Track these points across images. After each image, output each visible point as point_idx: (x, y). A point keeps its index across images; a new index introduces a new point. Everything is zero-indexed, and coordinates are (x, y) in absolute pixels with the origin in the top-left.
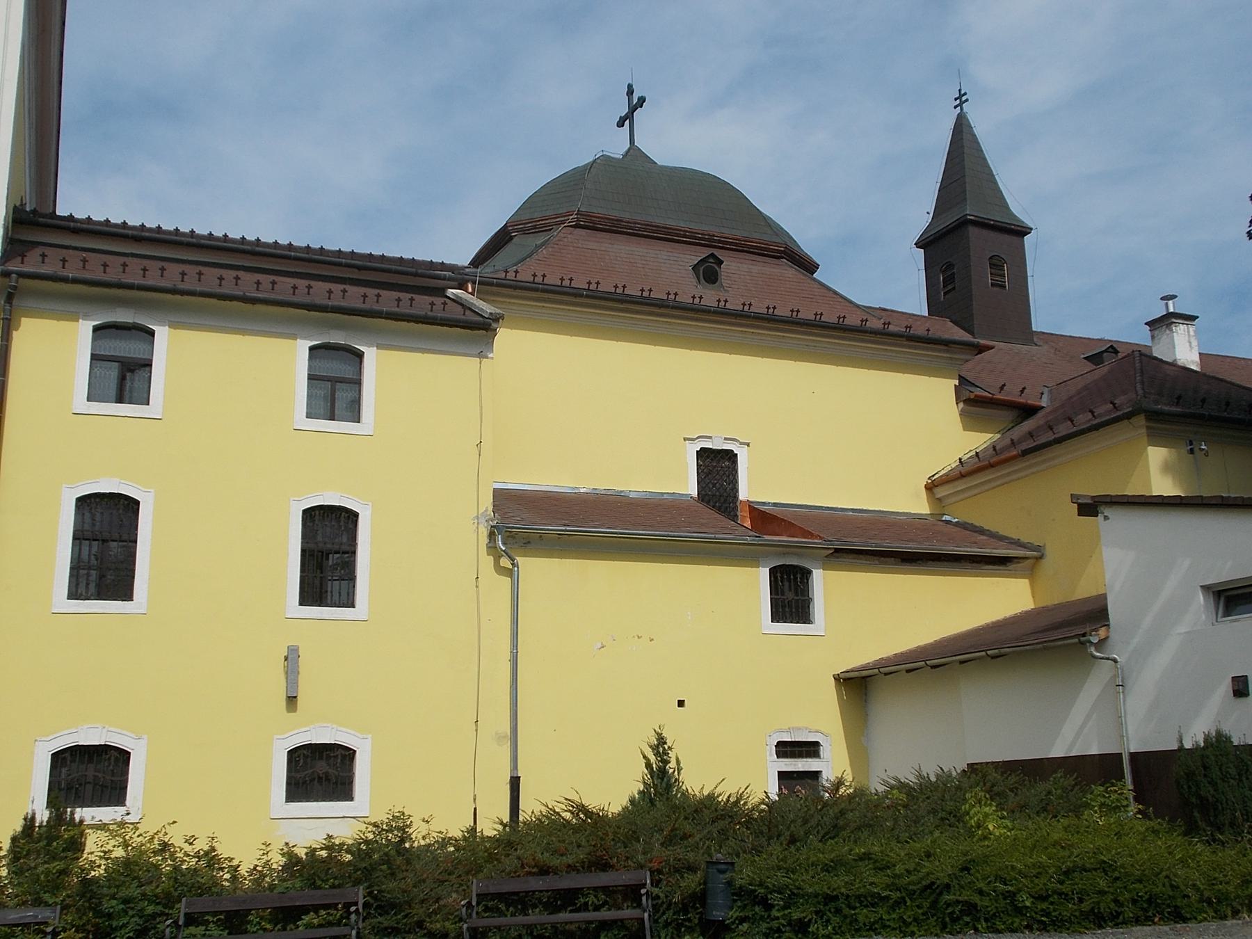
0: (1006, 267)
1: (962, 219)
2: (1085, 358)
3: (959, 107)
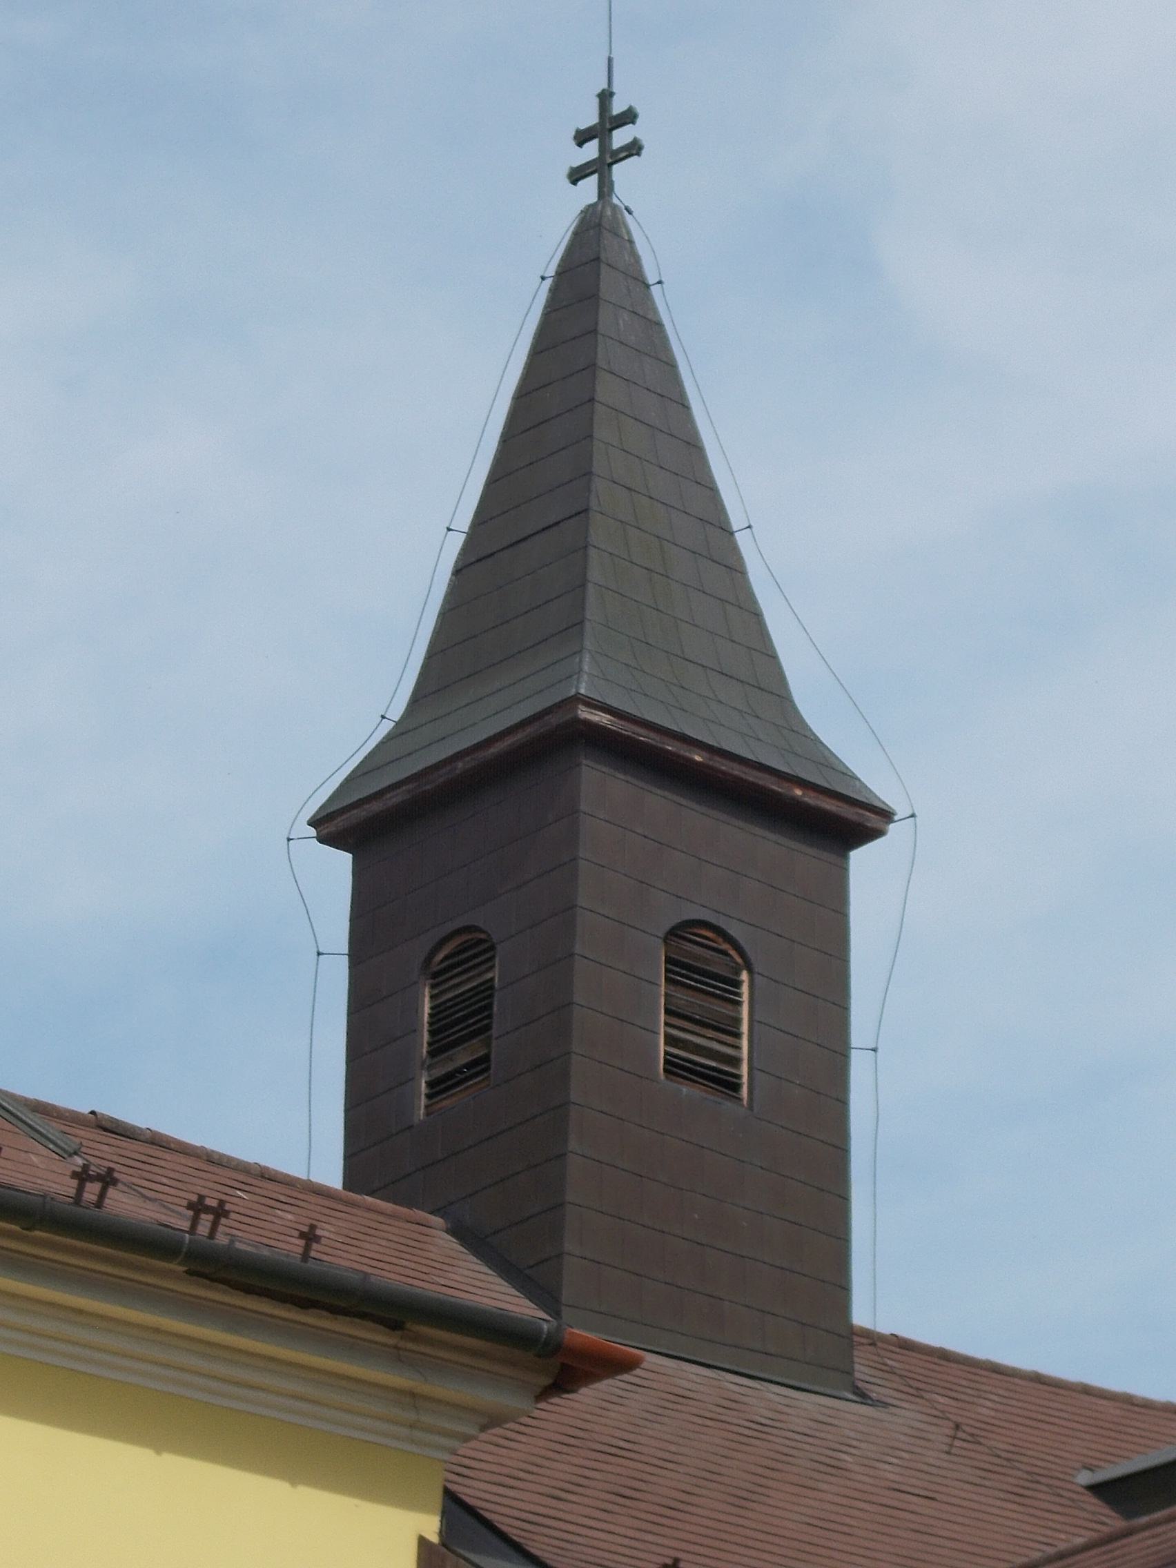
0: (745, 989)
1: (554, 720)
2: (1096, 1489)
3: (595, 177)
